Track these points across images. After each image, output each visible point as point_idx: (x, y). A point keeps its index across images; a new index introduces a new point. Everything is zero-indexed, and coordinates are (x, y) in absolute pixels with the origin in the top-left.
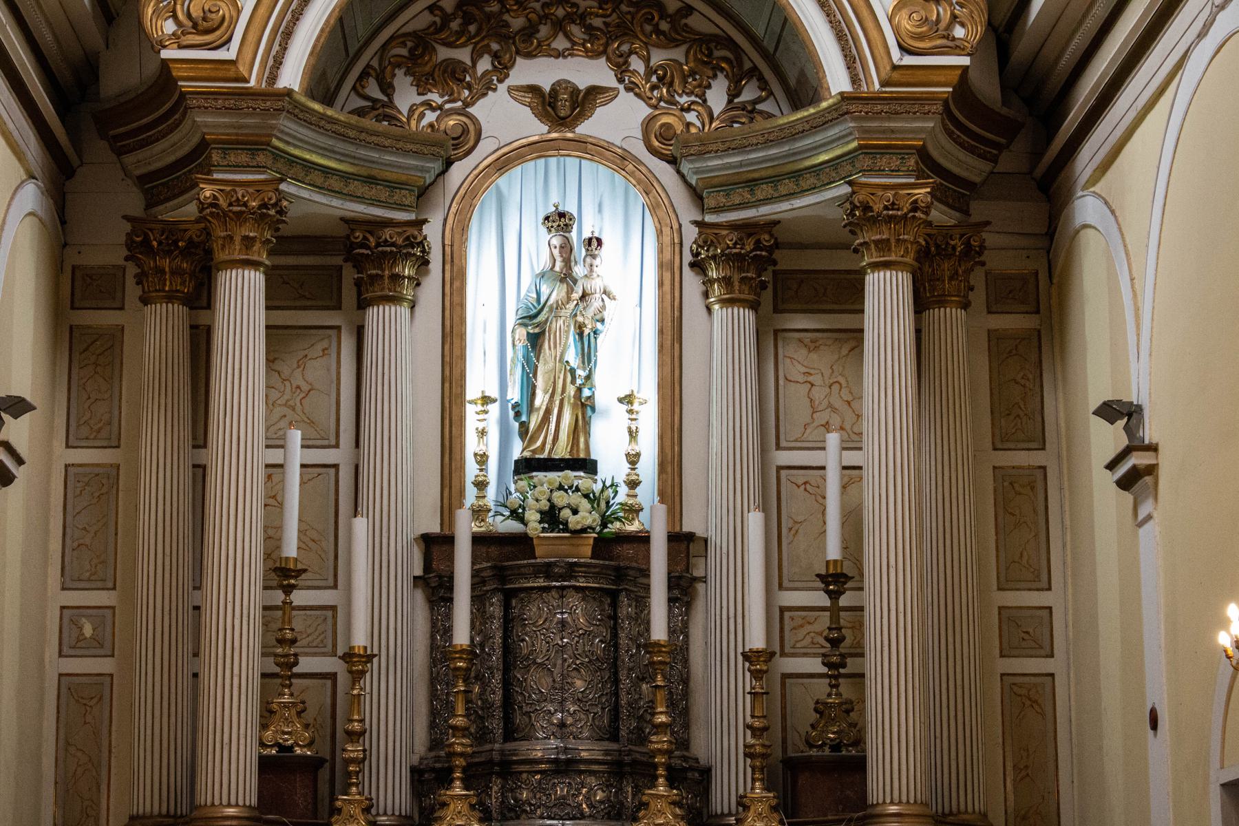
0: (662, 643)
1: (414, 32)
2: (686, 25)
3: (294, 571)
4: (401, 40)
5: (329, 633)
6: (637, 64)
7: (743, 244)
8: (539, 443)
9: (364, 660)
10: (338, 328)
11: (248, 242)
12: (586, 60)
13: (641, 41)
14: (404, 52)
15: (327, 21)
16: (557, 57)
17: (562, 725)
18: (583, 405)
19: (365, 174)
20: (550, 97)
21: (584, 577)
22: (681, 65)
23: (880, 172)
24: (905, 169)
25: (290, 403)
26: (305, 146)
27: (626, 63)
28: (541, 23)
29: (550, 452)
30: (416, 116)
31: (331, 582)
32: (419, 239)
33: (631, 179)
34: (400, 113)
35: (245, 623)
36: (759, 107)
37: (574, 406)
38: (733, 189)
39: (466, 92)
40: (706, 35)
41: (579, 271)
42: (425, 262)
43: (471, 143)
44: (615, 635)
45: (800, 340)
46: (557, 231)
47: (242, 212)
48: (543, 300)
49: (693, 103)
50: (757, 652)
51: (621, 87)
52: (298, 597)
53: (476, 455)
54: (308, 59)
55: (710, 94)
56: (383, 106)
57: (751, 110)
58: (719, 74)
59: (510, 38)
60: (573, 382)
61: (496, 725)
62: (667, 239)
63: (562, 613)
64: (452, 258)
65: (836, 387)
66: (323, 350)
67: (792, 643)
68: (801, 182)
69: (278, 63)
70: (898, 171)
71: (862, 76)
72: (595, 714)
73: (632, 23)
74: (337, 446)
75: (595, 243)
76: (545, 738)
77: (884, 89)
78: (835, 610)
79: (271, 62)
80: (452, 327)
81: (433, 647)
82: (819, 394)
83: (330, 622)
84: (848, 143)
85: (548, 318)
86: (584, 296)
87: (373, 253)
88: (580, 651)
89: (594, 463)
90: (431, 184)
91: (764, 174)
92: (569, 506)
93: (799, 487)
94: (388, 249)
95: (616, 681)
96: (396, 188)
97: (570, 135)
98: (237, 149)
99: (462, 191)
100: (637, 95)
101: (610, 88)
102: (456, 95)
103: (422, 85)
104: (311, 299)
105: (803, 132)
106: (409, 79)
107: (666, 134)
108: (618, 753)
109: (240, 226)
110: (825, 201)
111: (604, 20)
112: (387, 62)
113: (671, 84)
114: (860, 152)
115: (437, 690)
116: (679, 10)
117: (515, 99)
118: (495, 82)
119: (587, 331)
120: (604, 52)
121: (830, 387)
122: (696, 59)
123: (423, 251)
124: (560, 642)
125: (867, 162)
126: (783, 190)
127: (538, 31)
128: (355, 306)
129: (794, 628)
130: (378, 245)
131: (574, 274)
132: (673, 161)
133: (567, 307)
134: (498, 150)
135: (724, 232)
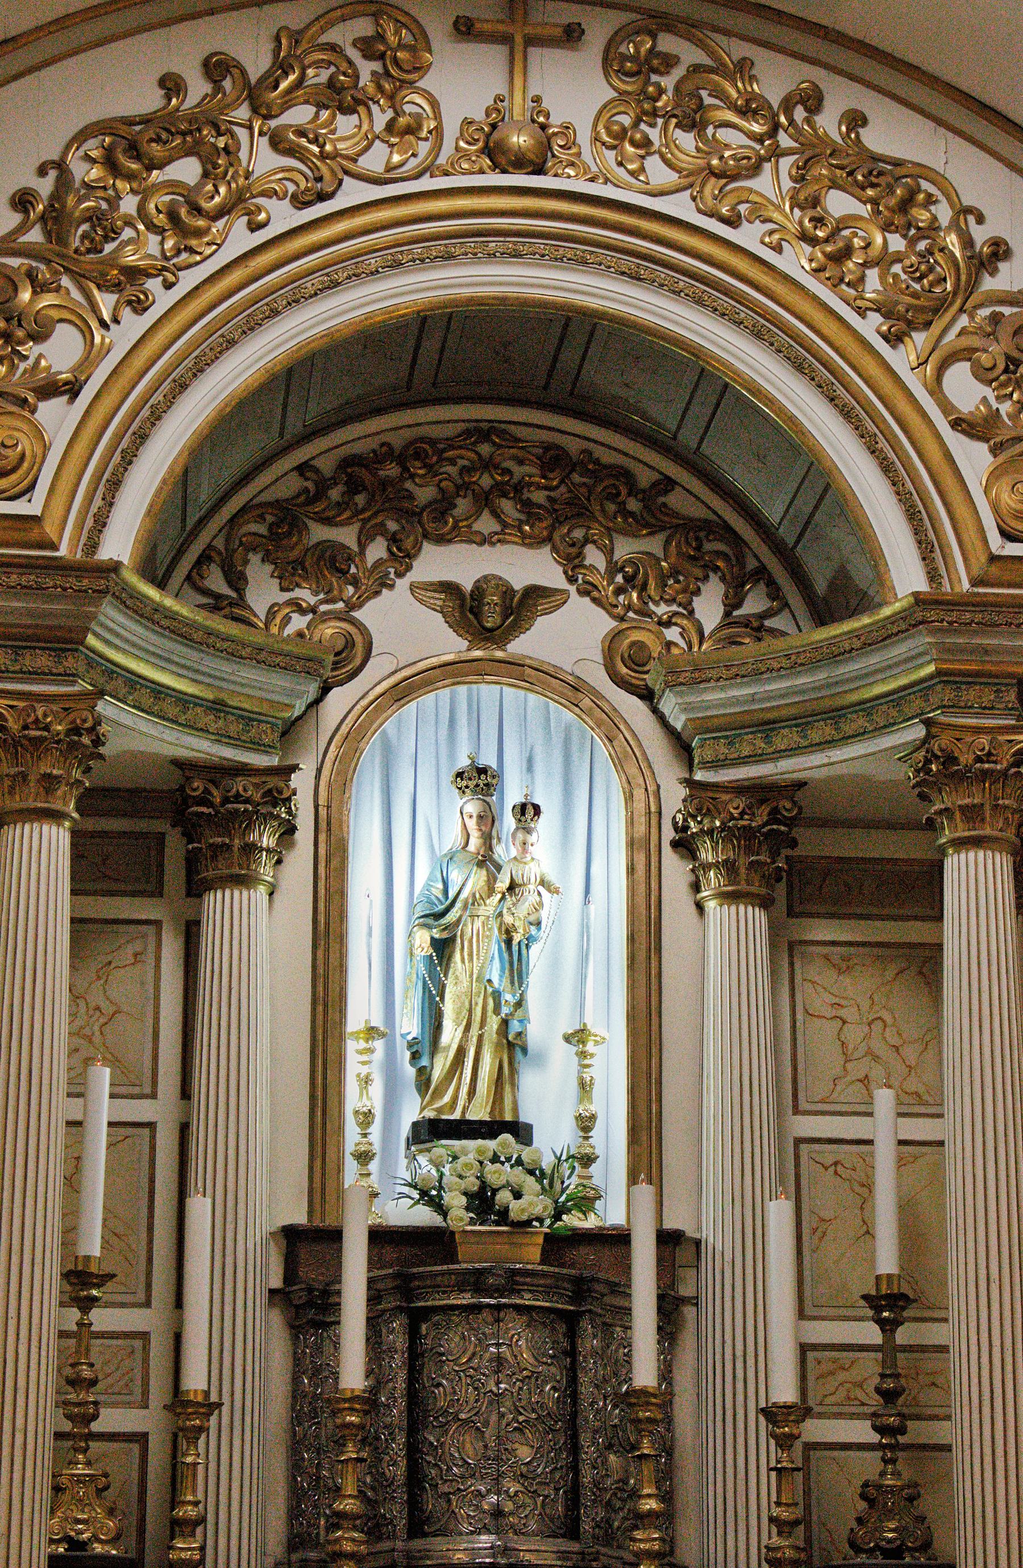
0: (651, 1390)
1: (277, 501)
2: (664, 505)
3: (97, 1276)
4: (258, 512)
5: (138, 1373)
6: (594, 557)
7: (753, 814)
8: (447, 1098)
9: (202, 1410)
10: (157, 924)
11: (49, 783)
12: (524, 549)
13: (600, 523)
14: (262, 529)
15: (171, 468)
16: (481, 544)
17: (498, 1513)
18: (511, 1045)
19: (211, 697)
20: (473, 599)
21: (530, 1291)
22: (658, 560)
23: (966, 709)
24: (1002, 706)
25: (83, 1031)
26: (132, 650)
27: (580, 555)
28: (458, 496)
29: (463, 1113)
30: (278, 621)
31: (141, 1297)
32: (285, 795)
33: (587, 719)
34: (256, 615)
35: (34, 1350)
36: (767, 623)
37: (498, 1046)
38: (740, 735)
39: (351, 590)
40: (691, 520)
41: (500, 852)
42: (289, 830)
43: (358, 661)
44: (573, 1380)
45: (826, 957)
46: (475, 792)
47: (41, 740)
48: (452, 894)
49: (676, 614)
50: (784, 1407)
51: (572, 589)
52: (101, 1319)
53: (356, 1112)
54: (143, 520)
55: (697, 603)
56: (231, 605)
57: (756, 627)
58: (711, 574)
59: (414, 514)
60: (497, 1010)
61: (396, 1512)
62: (640, 806)
63: (498, 1345)
64: (329, 824)
65: (878, 1026)
66: (136, 955)
67: (819, 1398)
68: (841, 725)
69: (101, 523)
70: (992, 708)
71: (943, 571)
72: (546, 1497)
73: (589, 500)
74: (153, 1096)
75: (530, 812)
76: (472, 1533)
77: (976, 590)
78: (888, 1350)
79: (90, 522)
80: (327, 924)
81: (296, 1394)
82: (854, 1034)
83: (139, 1355)
84: (921, 666)
85: (460, 917)
86: (512, 888)
87: (217, 812)
88: (524, 1403)
89: (529, 1128)
90: (299, 718)
91: (785, 713)
92: (507, 1185)
93: (826, 1168)
94: (242, 807)
95: (575, 1449)
96: (254, 720)
97: (499, 654)
98: (34, 648)
99: (344, 729)
100: (594, 600)
101: (557, 590)
102: (335, 592)
103: (287, 576)
104: (116, 880)
105: (850, 651)
106: (269, 568)
107: (638, 658)
108: (579, 1557)
109: (39, 758)
110: (880, 751)
111: (547, 493)
112: (237, 542)
113: (644, 587)
114: (937, 680)
115: (303, 1459)
116: (654, 485)
117: (420, 601)
118: (392, 576)
119: (517, 938)
120: (549, 539)
121: (870, 1024)
122: (680, 553)
123: (289, 812)
124: (494, 1389)
125: (948, 695)
126: (815, 736)
127: (455, 506)
128: (183, 891)
129: (822, 1376)
130: (226, 800)
131: (496, 857)
132: (648, 696)
133: (488, 902)
134: (396, 672)
135: (725, 797)
